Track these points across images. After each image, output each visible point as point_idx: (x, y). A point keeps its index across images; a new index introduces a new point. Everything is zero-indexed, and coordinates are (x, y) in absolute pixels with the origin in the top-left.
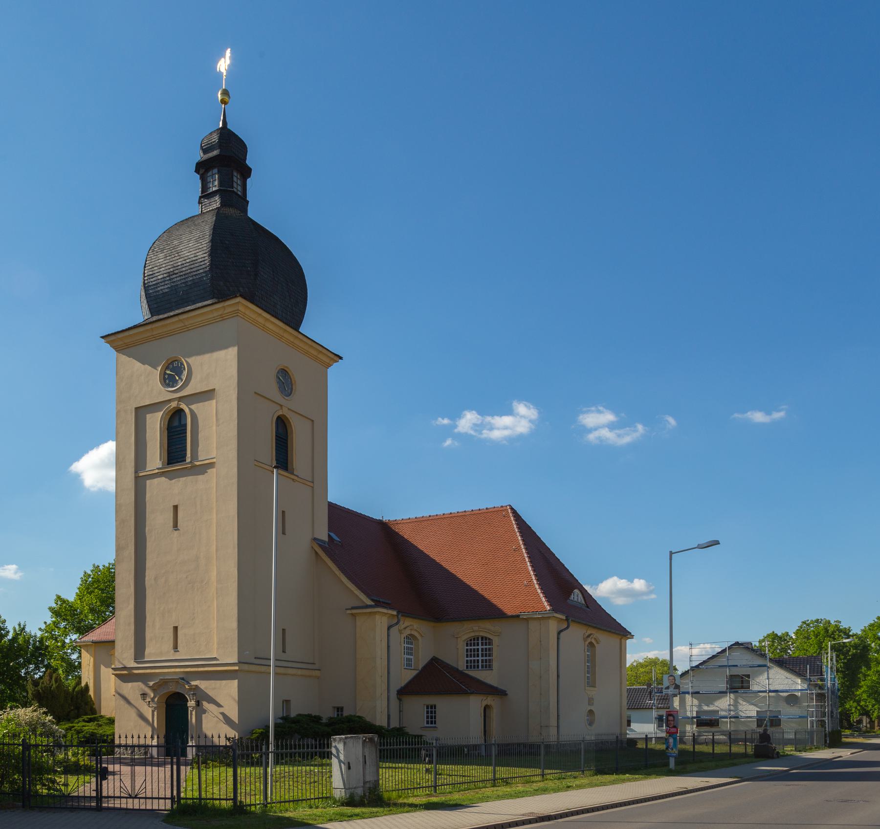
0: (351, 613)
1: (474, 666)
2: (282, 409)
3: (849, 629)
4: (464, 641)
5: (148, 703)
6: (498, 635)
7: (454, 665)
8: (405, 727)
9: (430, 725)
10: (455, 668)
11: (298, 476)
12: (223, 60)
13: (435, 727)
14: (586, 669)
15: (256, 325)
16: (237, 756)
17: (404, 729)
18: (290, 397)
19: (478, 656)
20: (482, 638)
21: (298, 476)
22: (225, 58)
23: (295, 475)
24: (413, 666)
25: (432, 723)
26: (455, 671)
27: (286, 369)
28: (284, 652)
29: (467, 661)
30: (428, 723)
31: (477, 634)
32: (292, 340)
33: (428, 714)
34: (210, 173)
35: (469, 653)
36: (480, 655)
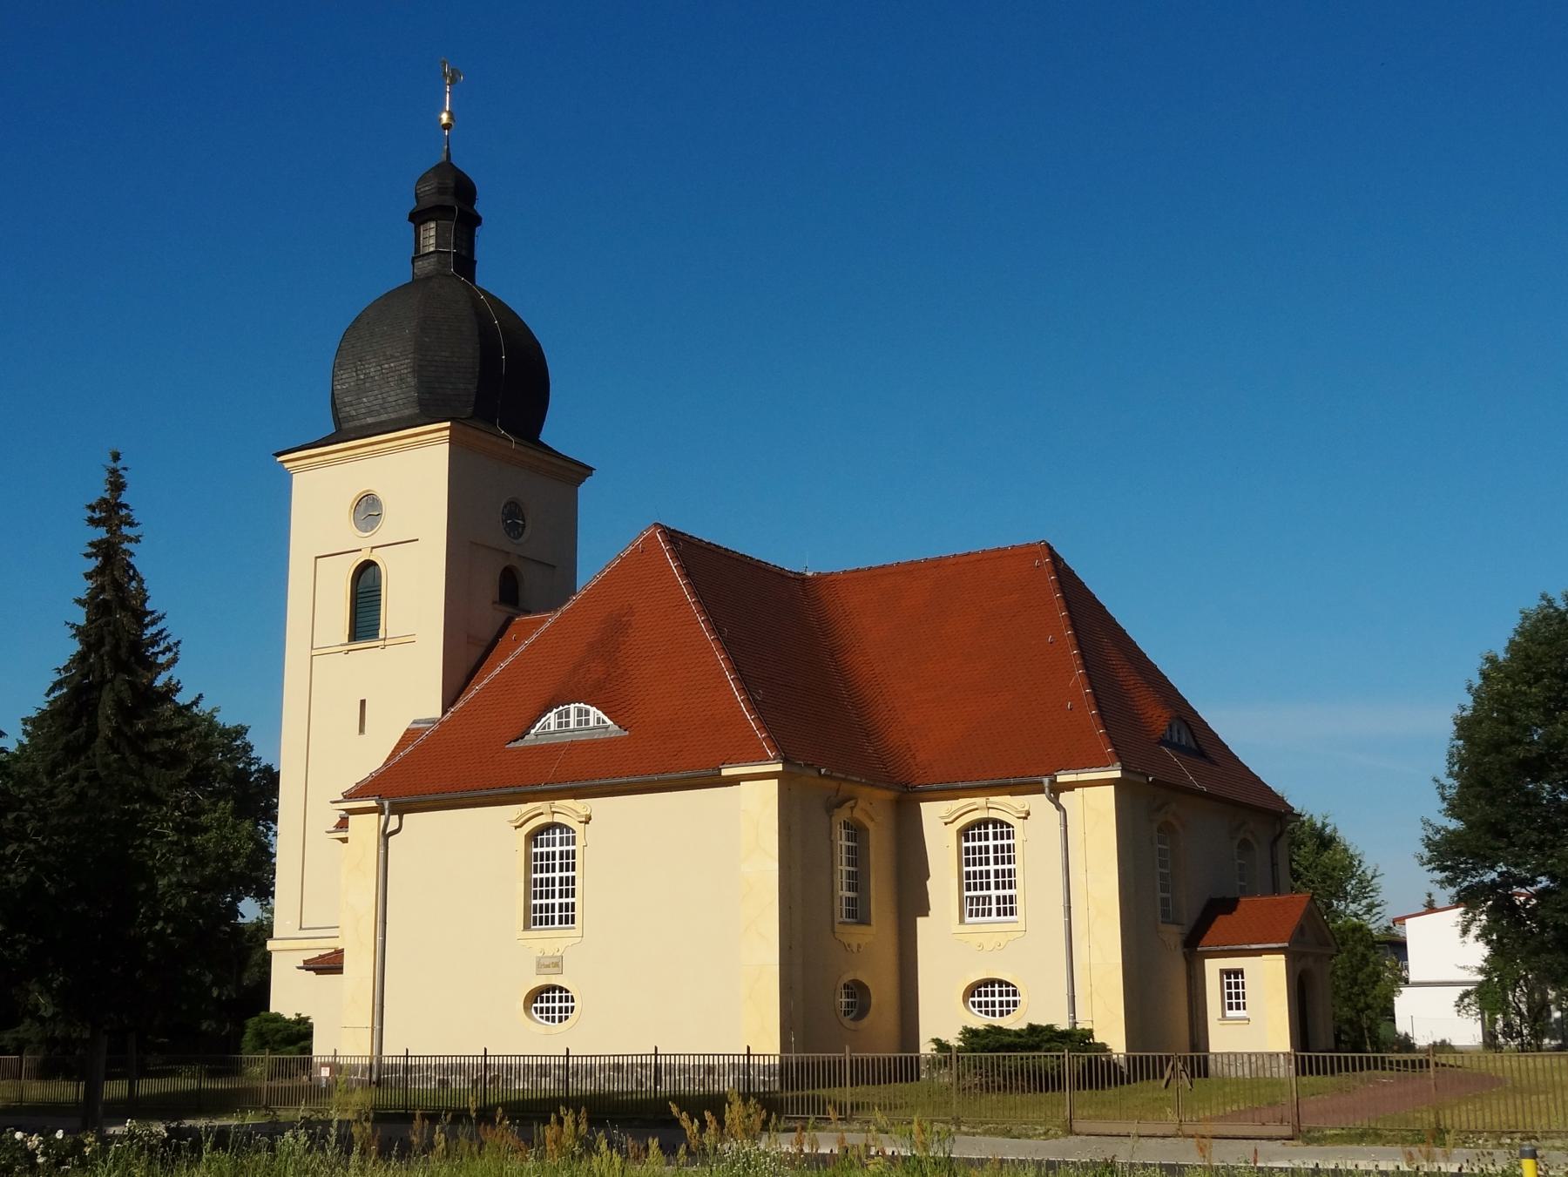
25: (1238, 1008)
33: (1235, 982)
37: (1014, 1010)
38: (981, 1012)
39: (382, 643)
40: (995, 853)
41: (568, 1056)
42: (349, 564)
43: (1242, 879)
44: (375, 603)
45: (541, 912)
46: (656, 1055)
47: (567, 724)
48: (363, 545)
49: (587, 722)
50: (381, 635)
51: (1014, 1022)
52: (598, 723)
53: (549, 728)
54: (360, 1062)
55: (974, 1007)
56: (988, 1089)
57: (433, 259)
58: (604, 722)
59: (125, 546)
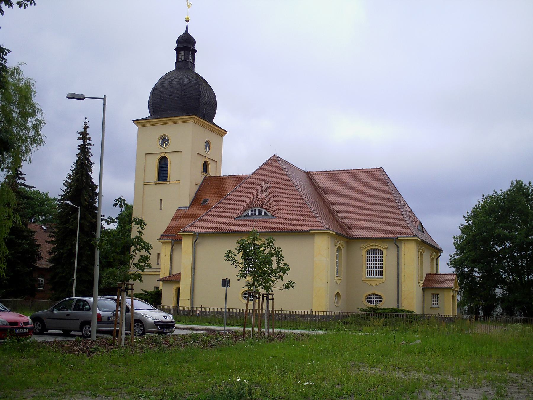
3: (10, 125)
4: (366, 251)
6: (386, 249)
13: (438, 307)
14: (336, 257)
16: (252, 305)
19: (374, 261)
20: (376, 250)
25: (436, 304)
29: (367, 263)
30: (433, 304)
31: (374, 247)
34: (180, 52)
35: (377, 259)
36: (375, 260)
37: (380, 303)
38: (369, 303)
39: (169, 182)
40: (376, 258)
41: (282, 310)
42: (156, 158)
43: (337, 267)
44: (166, 171)
45: (370, 272)
46: (311, 311)
47: (255, 214)
48: (163, 151)
49: (261, 213)
50: (168, 180)
51: (379, 306)
52: (265, 214)
53: (249, 214)
54: (168, 308)
55: (367, 301)
56: (527, 322)
57: (183, 63)
58: (267, 214)
59: (89, 146)
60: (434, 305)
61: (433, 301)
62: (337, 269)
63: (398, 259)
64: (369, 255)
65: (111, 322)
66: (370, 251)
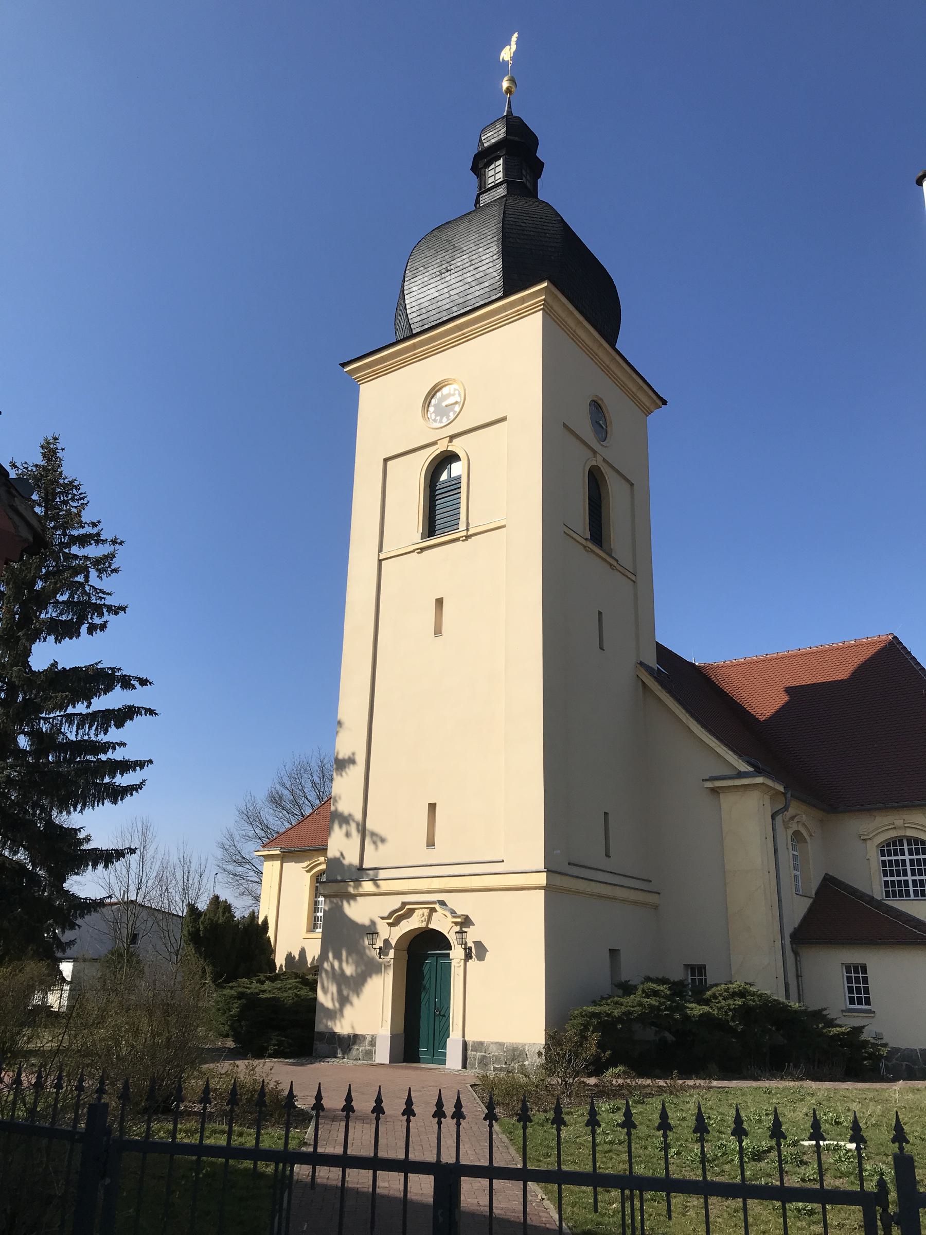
0: (712, 786)
1: (900, 892)
2: (595, 457)
4: (878, 846)
5: (378, 950)
7: (868, 892)
8: (825, 1009)
9: (857, 1007)
10: (868, 896)
11: (617, 560)
12: (508, 47)
13: (870, 1011)
15: (565, 329)
17: (824, 1013)
18: (606, 441)
21: (617, 560)
22: (510, 45)
23: (613, 558)
24: (801, 891)
25: (860, 1003)
26: (871, 900)
27: (600, 402)
28: (431, 843)
30: (852, 1001)
31: (901, 833)
32: (608, 363)
60: (856, 1005)
61: (850, 990)
62: (795, 876)
63: (633, 878)
64: (887, 858)
65: (586, 350)
66: (888, 845)
